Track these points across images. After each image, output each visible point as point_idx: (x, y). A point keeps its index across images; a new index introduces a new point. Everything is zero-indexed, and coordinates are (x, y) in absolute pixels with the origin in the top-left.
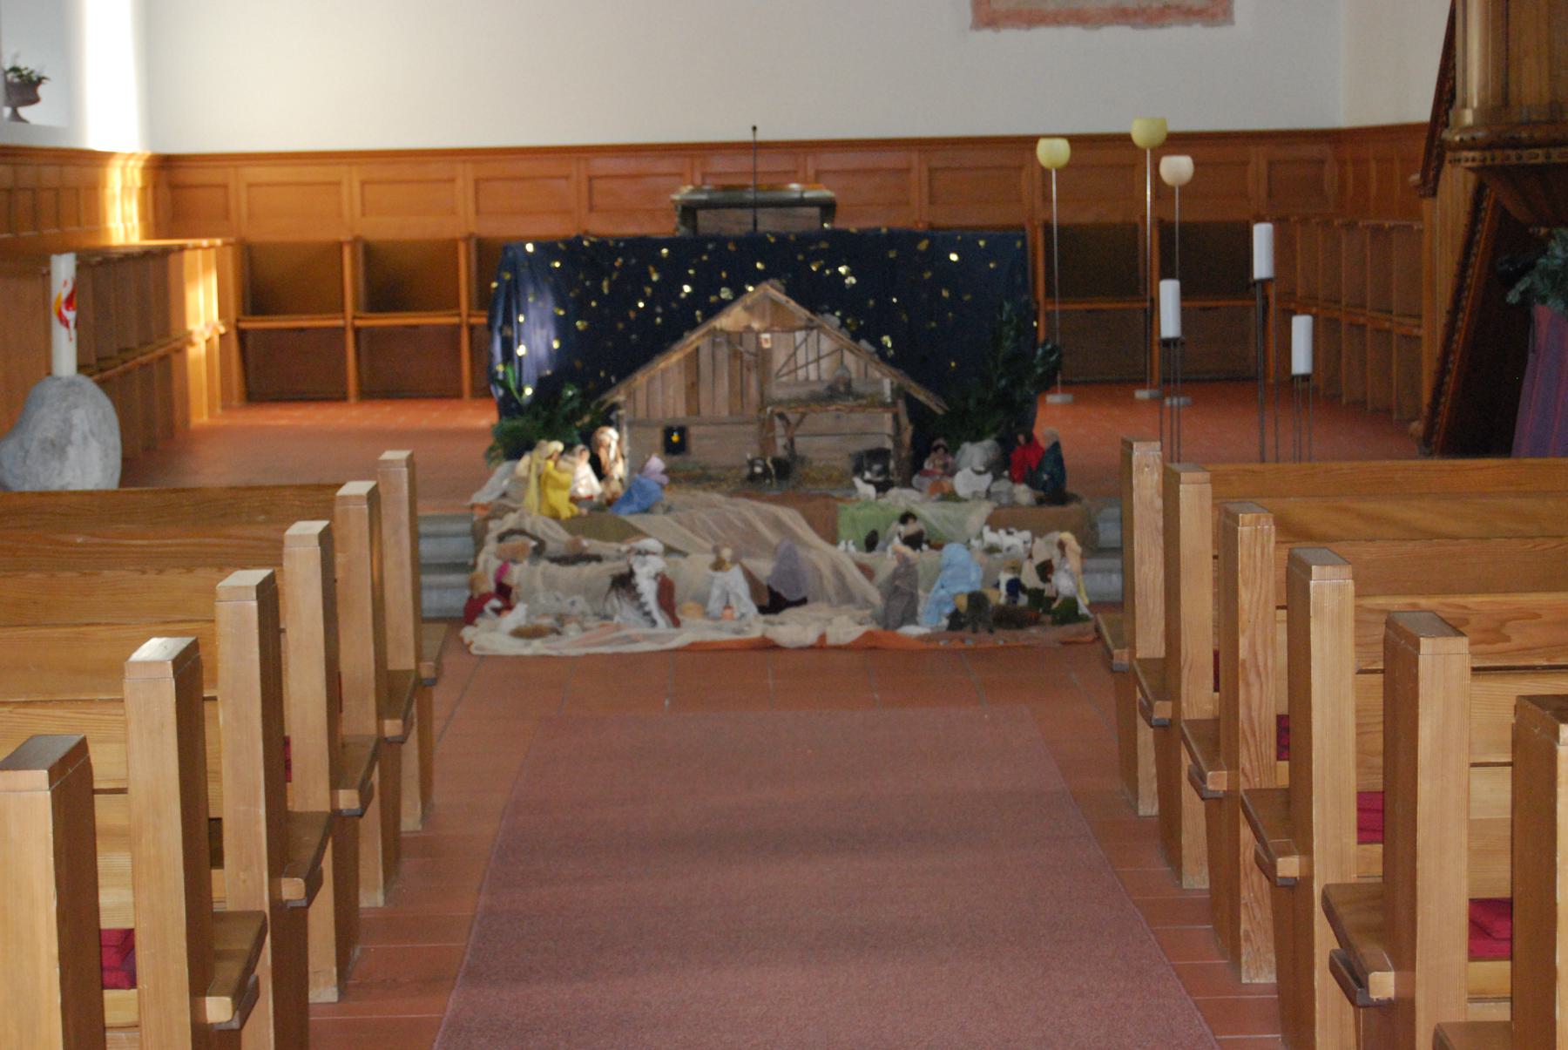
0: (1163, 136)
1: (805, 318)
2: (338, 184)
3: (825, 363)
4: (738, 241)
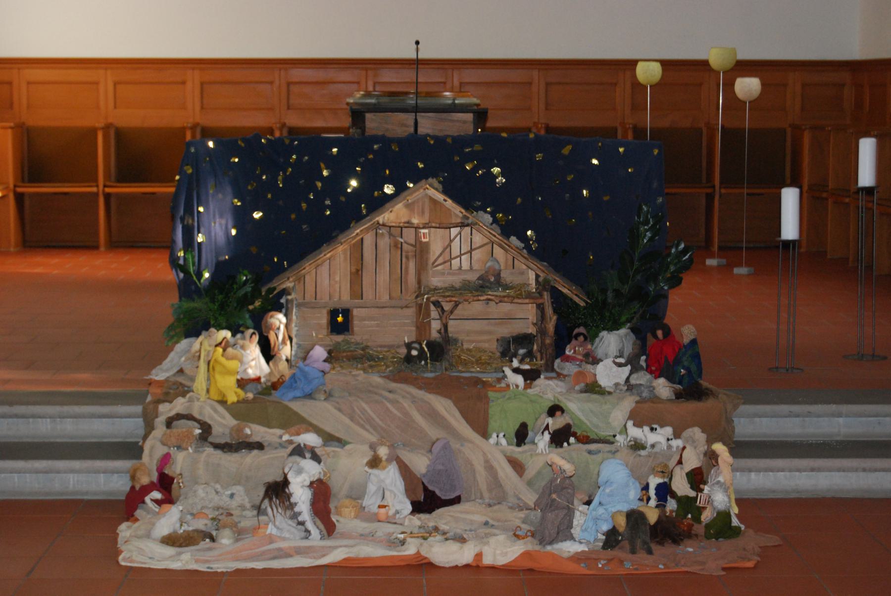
0: (734, 62)
1: (461, 215)
2: (97, 83)
3: (476, 254)
4: (399, 141)
